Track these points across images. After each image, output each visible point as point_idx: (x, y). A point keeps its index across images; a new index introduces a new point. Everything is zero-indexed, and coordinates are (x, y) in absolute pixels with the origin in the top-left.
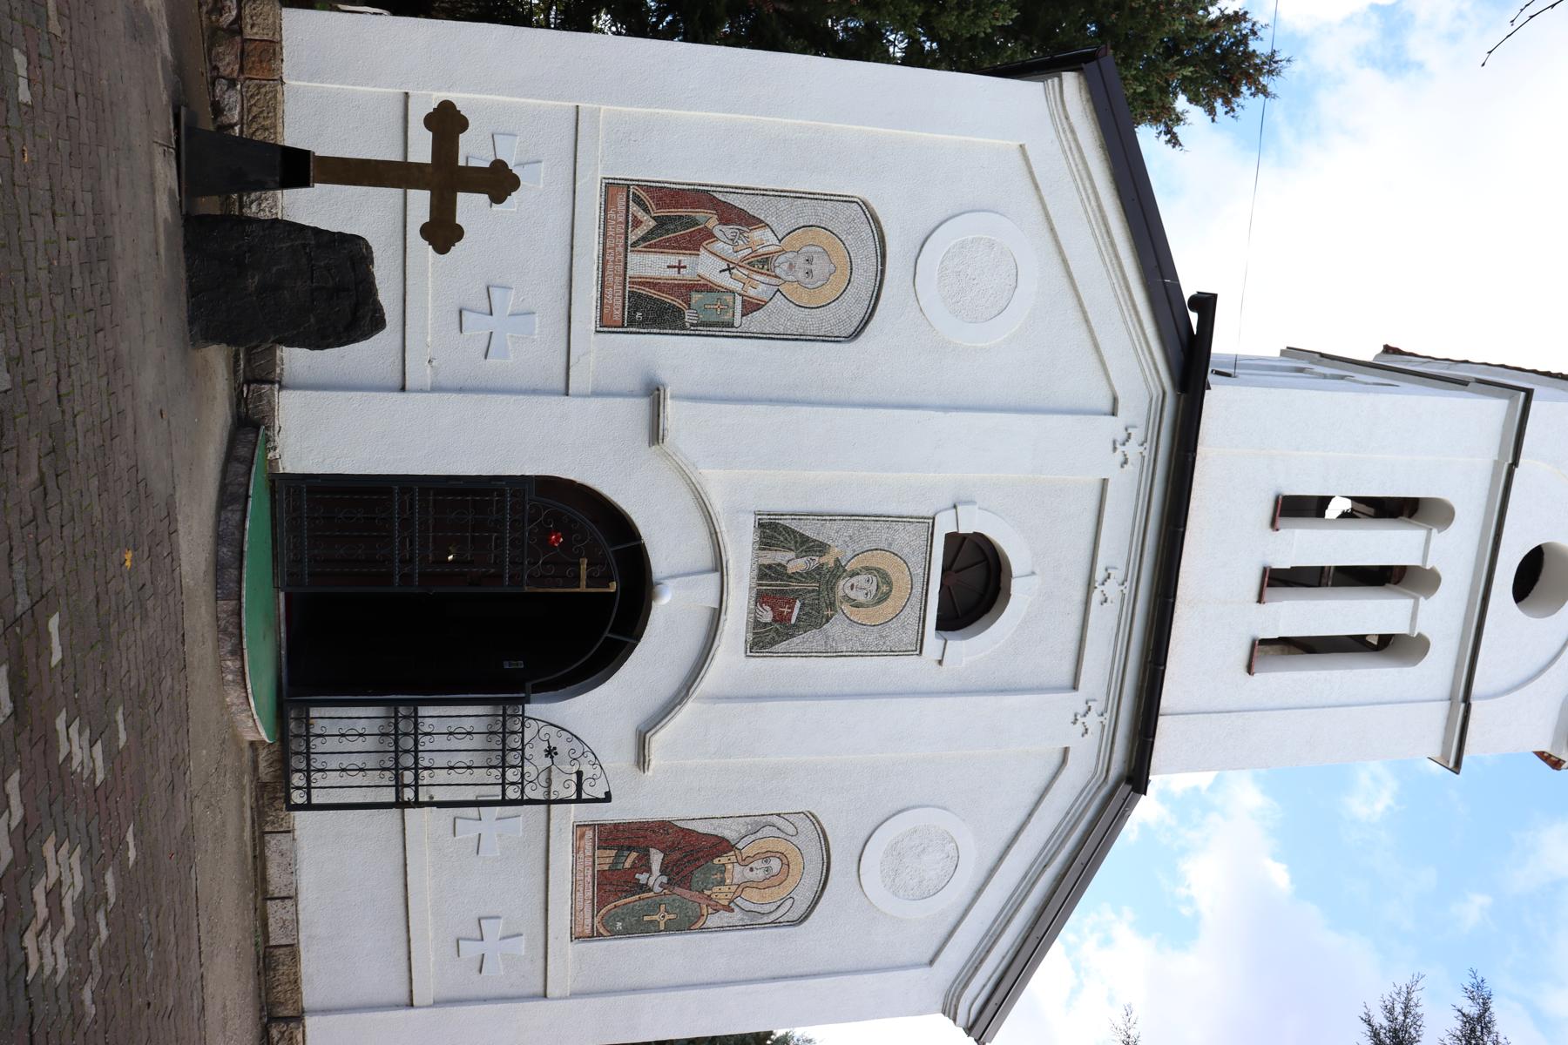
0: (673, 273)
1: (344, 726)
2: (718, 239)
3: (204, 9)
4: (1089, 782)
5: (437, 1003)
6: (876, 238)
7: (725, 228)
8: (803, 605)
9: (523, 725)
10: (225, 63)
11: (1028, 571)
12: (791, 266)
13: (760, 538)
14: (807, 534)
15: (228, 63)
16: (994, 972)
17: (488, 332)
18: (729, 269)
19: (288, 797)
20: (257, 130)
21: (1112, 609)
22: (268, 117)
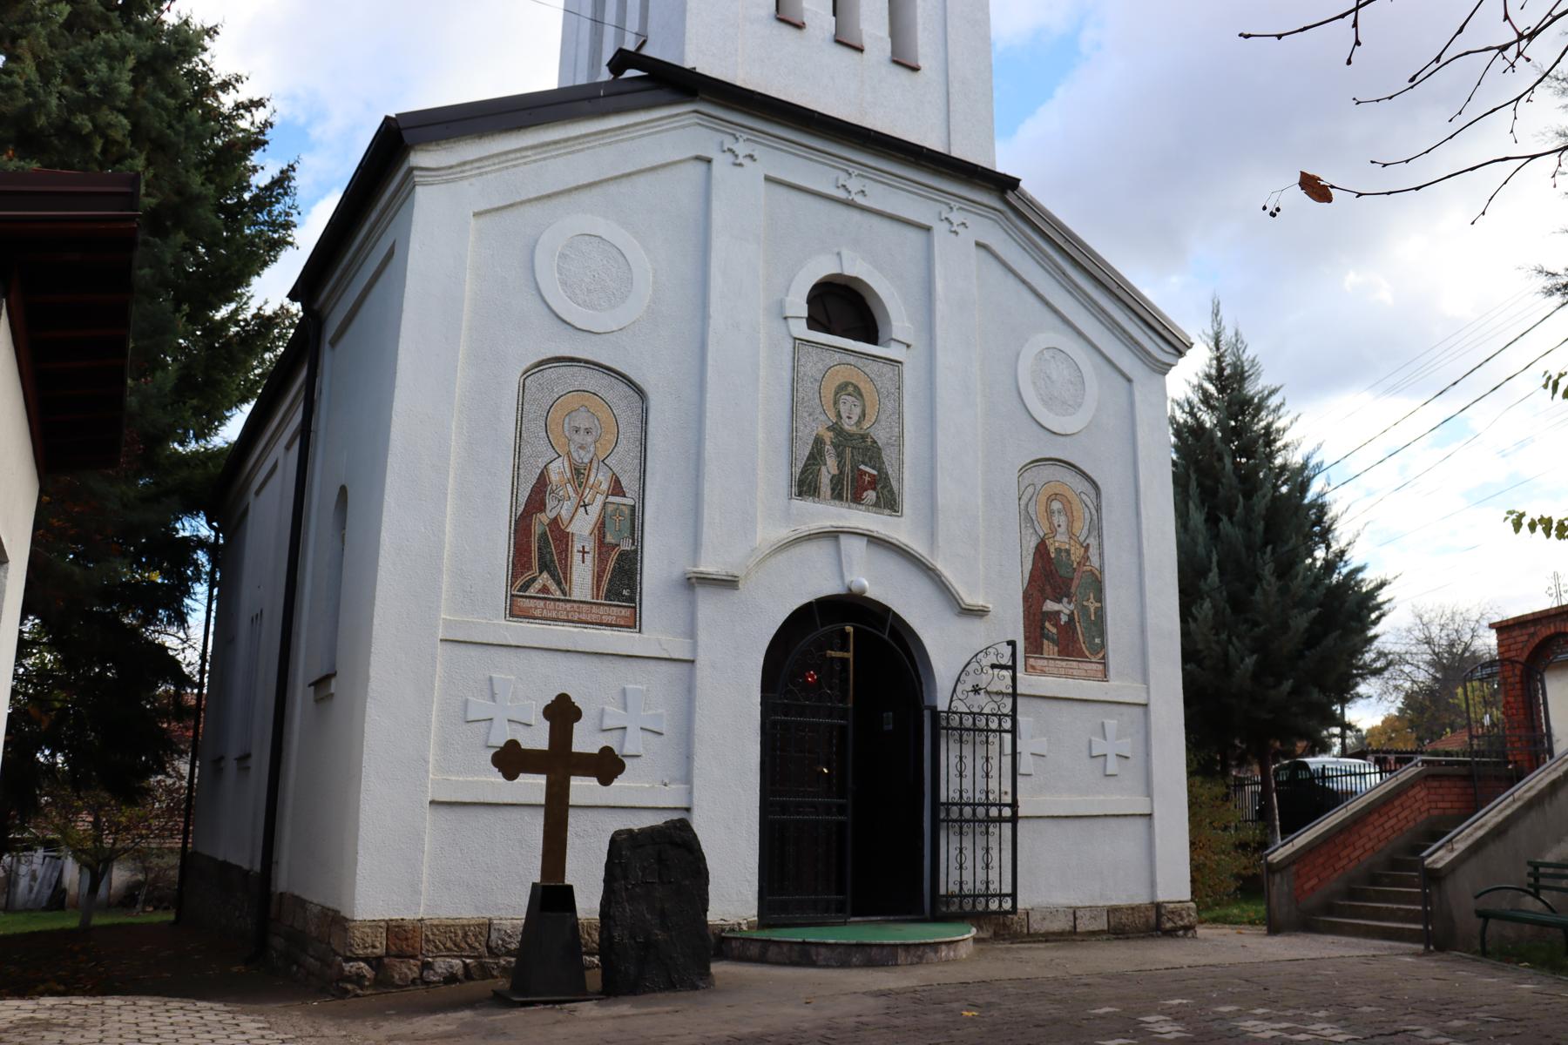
0: (588, 558)
1: (954, 864)
2: (559, 514)
3: (359, 992)
4: (1002, 227)
7: (549, 507)
8: (863, 463)
10: (409, 972)
11: (835, 258)
12: (582, 447)
14: (807, 454)
15: (410, 969)
17: (641, 733)
18: (585, 506)
19: (1007, 912)
20: (467, 942)
21: (871, 187)
22: (455, 933)
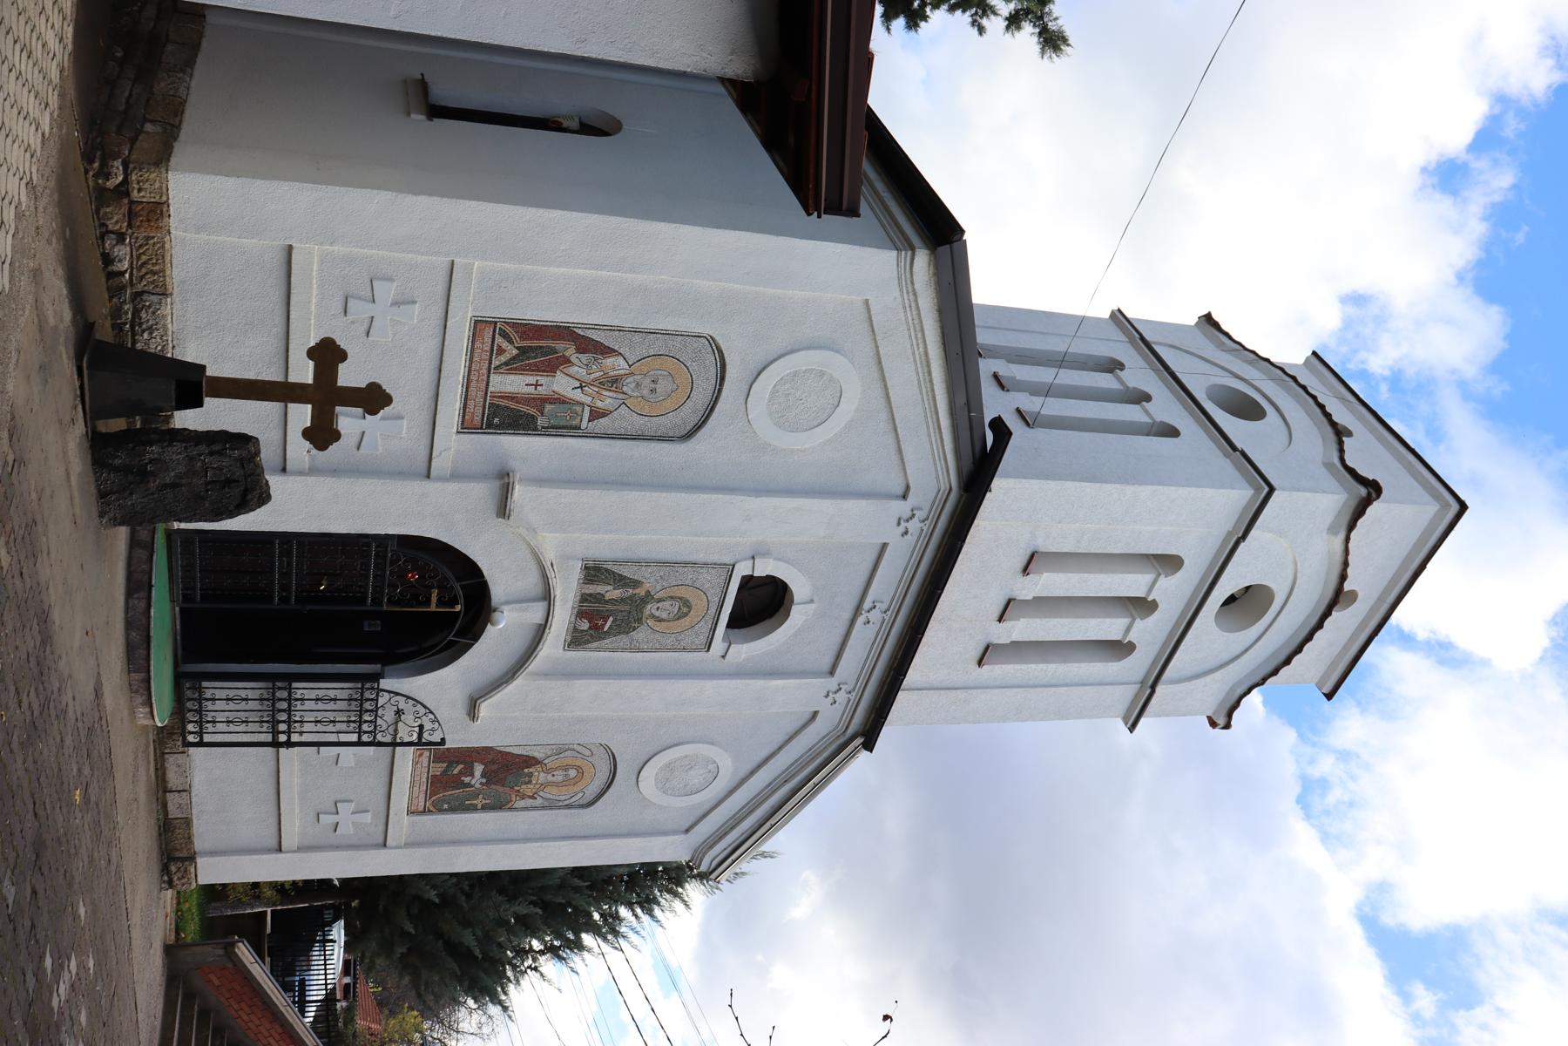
5: (300, 849)
6: (718, 364)
7: (580, 356)
9: (377, 695)
13: (585, 576)
15: (116, 220)
16: (734, 842)
18: (581, 387)
19: (184, 738)
20: (146, 274)
21: (870, 632)
22: (156, 264)
